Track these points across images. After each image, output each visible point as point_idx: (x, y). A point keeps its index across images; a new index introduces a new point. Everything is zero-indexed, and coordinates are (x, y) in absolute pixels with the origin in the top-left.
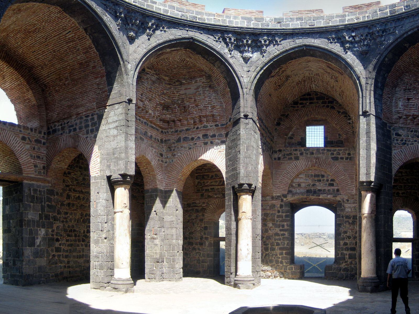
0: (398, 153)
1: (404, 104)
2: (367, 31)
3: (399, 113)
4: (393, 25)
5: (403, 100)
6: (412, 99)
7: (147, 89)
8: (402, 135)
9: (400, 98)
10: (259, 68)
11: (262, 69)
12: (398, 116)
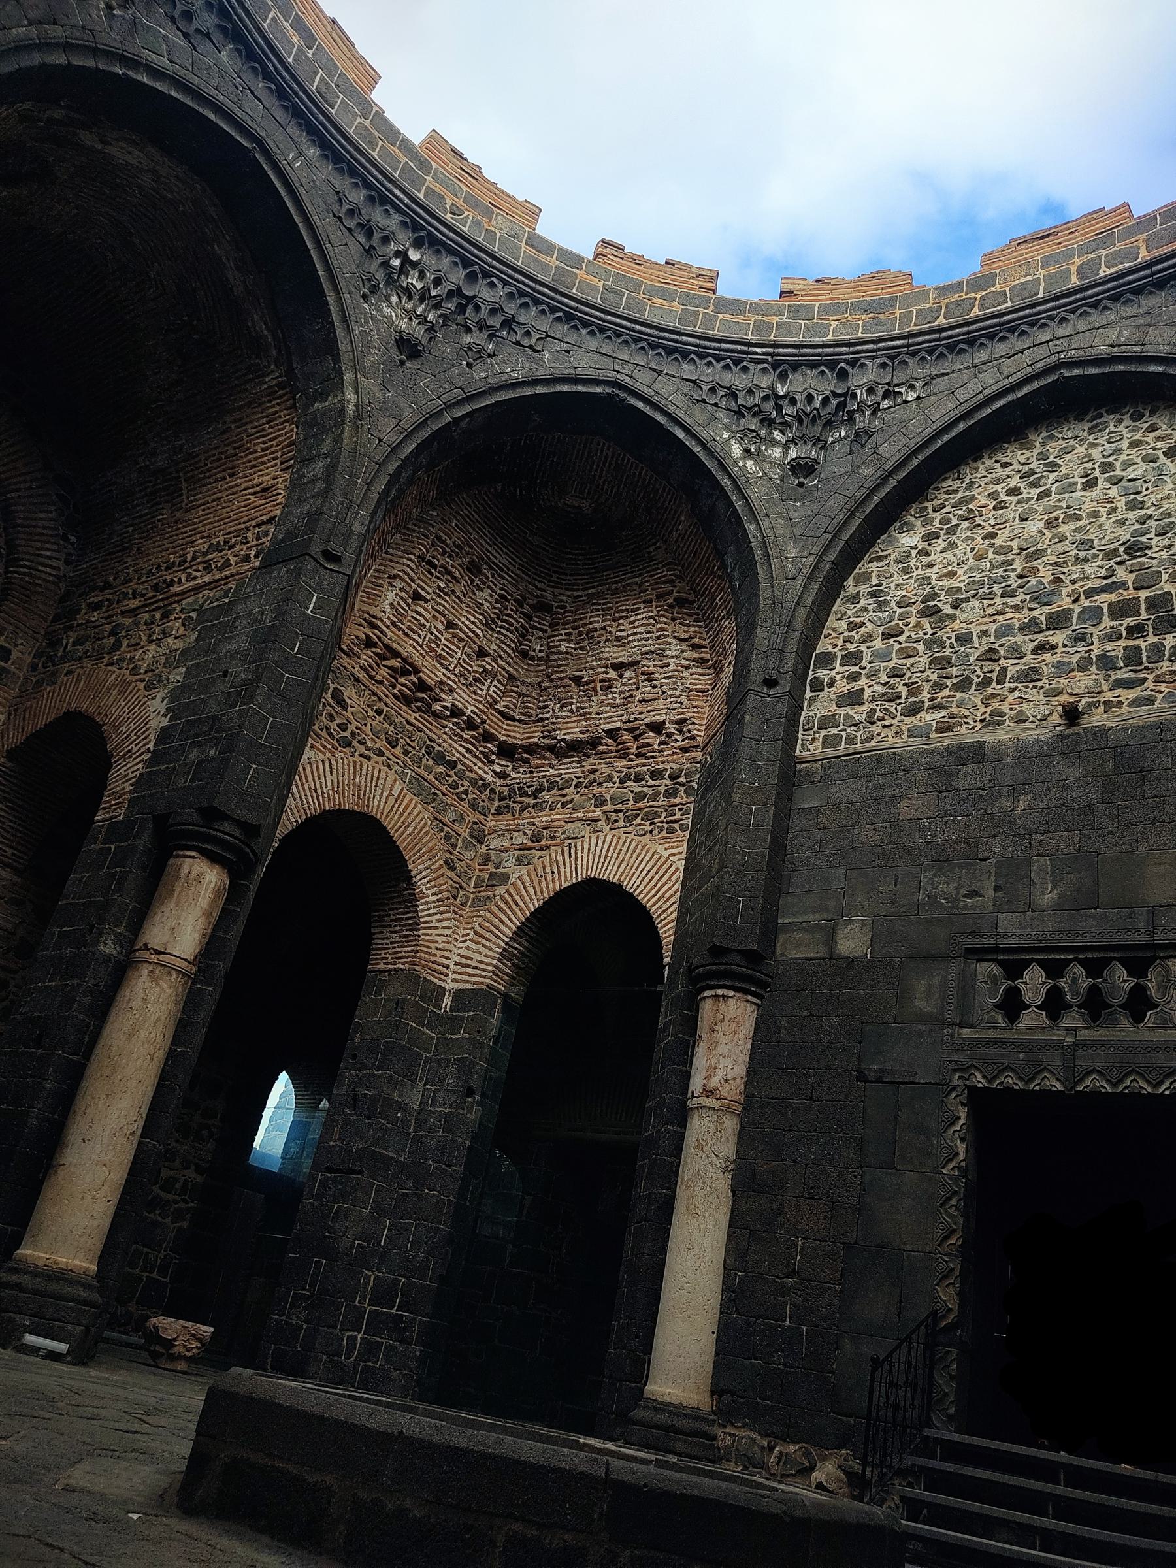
0: (320, 764)
1: (398, 603)
2: (457, 276)
3: (373, 626)
5: (402, 590)
6: (426, 601)
9: (395, 577)
12: (367, 636)
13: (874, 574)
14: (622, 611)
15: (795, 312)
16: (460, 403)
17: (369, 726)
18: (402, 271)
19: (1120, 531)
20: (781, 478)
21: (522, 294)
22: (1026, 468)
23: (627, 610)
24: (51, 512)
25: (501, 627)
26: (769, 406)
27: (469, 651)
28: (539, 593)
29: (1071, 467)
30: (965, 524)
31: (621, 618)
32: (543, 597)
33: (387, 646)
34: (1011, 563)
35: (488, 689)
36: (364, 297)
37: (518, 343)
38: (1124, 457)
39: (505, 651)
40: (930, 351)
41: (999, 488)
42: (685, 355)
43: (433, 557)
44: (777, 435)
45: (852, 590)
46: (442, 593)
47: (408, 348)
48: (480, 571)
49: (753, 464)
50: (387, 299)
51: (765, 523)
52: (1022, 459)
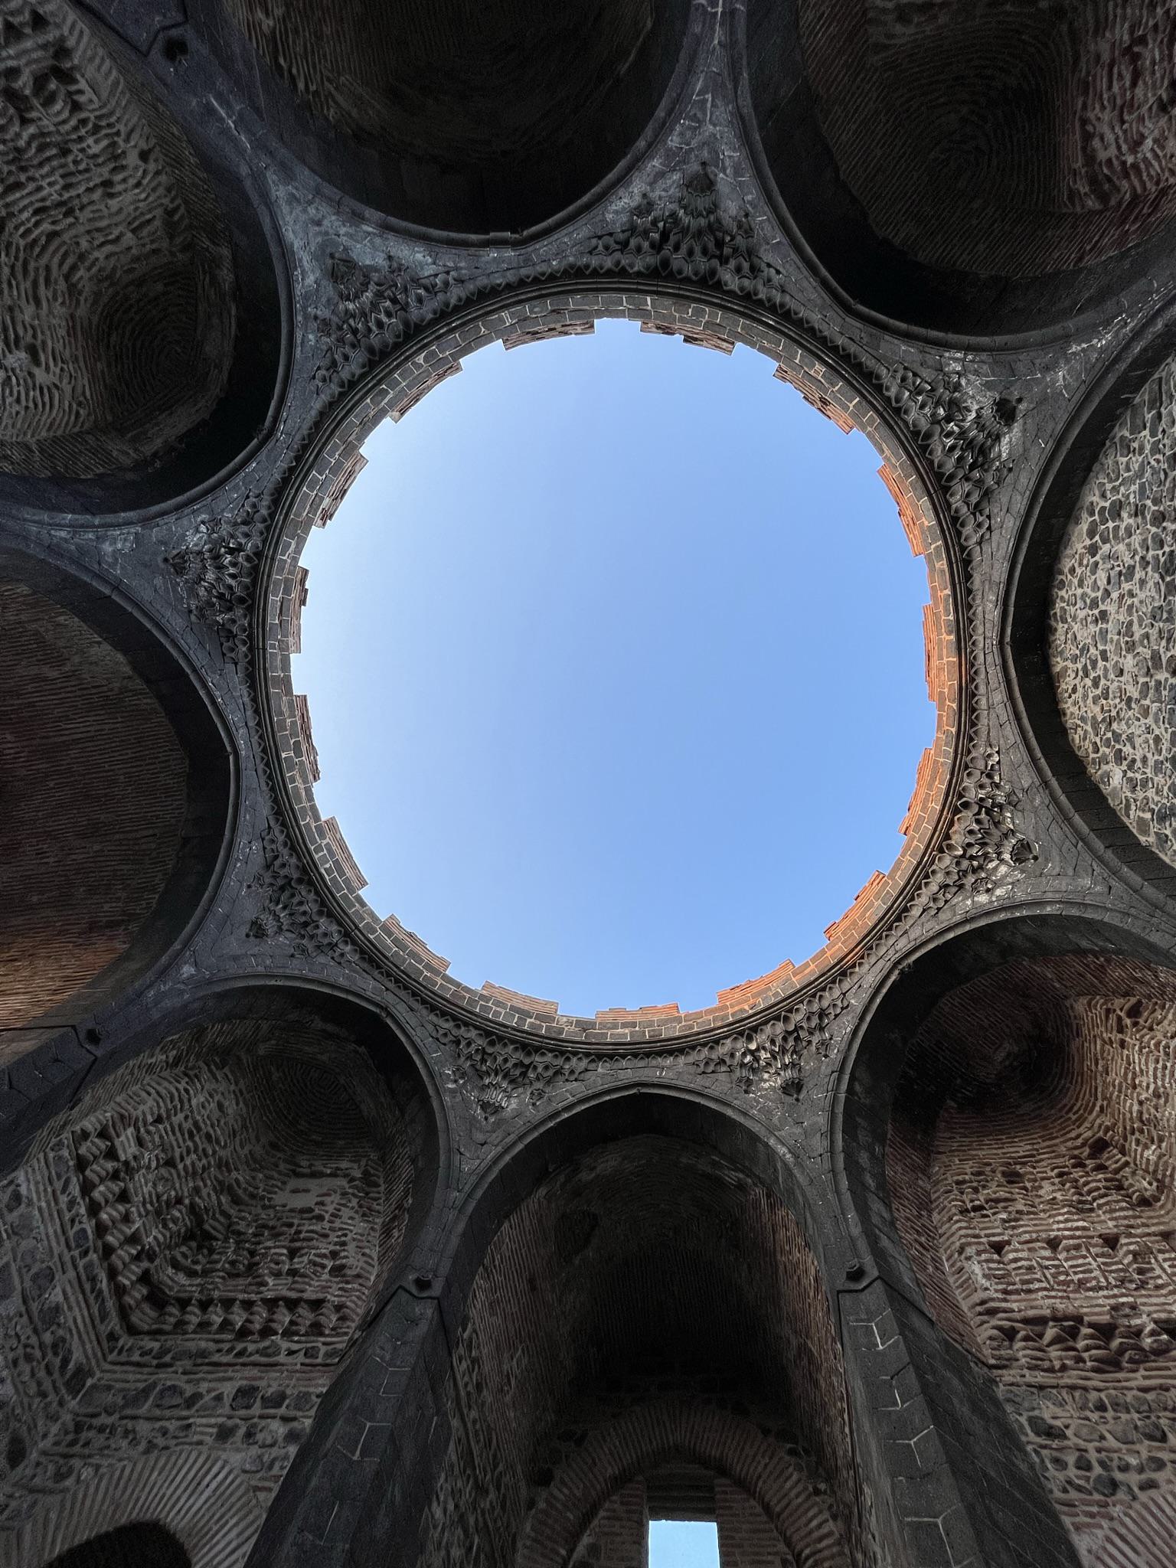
0: (1109, 1547)
1: (990, 1269)
2: (780, 1027)
3: (992, 1312)
4: (837, 993)
5: (979, 1253)
6: (1008, 1243)
7: (186, 1117)
8: (1069, 1433)
9: (961, 1251)
10: (513, 1137)
11: (521, 1138)
13: (1141, 815)
14: (1126, 1074)
15: (917, 828)
16: (839, 1080)
17: (1108, 1435)
18: (757, 1059)
19: (1151, 584)
20: (1022, 872)
21: (814, 996)
22: (1081, 673)
23: (1127, 1069)
24: (791, 1475)
25: (1094, 1200)
26: (965, 864)
27: (1098, 1250)
28: (1080, 1141)
29: (1085, 634)
30: (1115, 726)
31: (1133, 1079)
32: (1086, 1140)
33: (1026, 1321)
34: (1159, 683)
35: (1164, 1270)
36: (746, 1092)
37: (836, 1016)
38: (1089, 591)
39: (1125, 1218)
40: (971, 739)
41: (1091, 695)
42: (906, 910)
43: (972, 1201)
44: (991, 866)
45: (1152, 839)
46: (1010, 1223)
47: (793, 1088)
48: (1018, 1175)
49: (1004, 887)
50: (763, 1080)
51: (1049, 896)
52: (1073, 675)
